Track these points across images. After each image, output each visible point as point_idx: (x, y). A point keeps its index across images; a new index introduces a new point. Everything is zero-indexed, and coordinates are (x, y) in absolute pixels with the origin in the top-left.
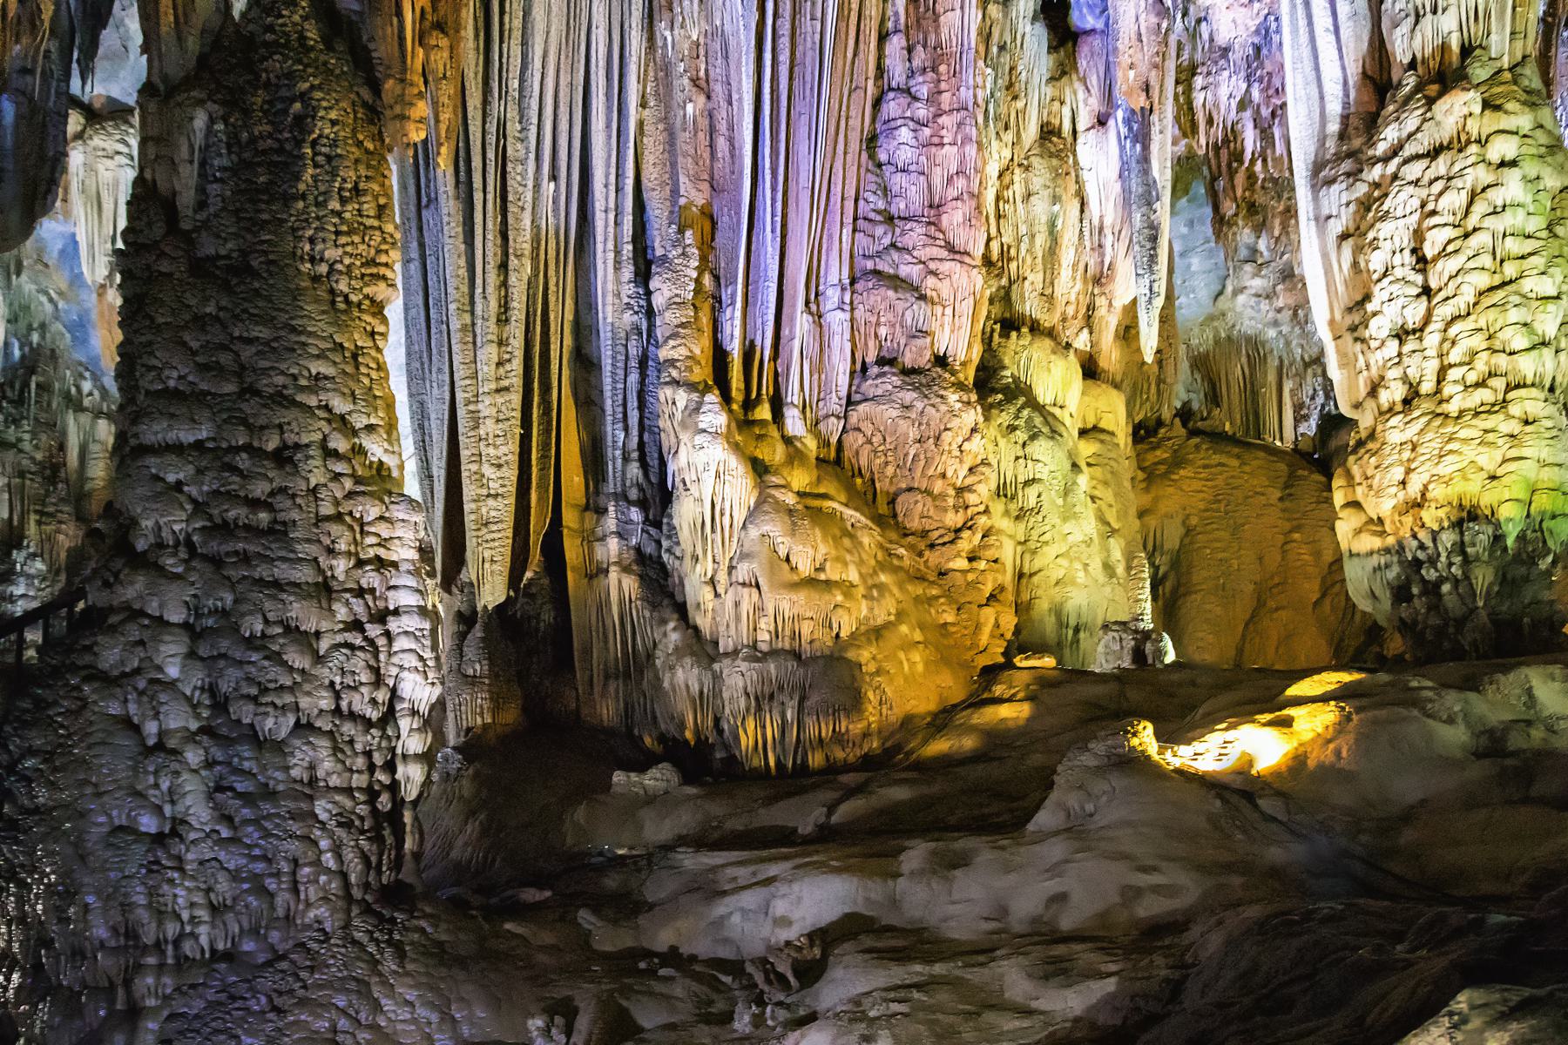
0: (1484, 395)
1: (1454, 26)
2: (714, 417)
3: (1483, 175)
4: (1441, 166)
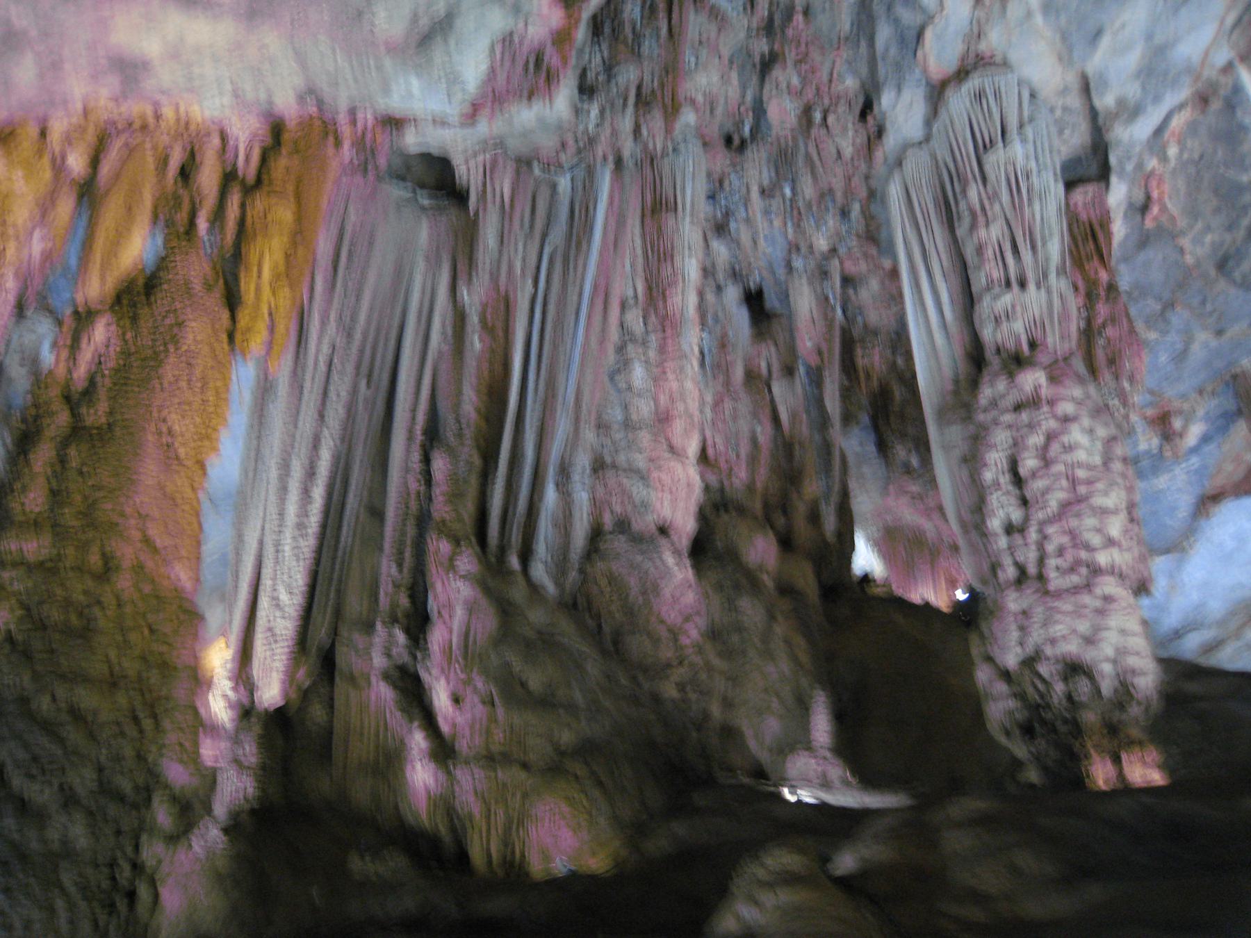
0: (1075, 579)
1: (1022, 331)
2: (467, 562)
3: (1053, 424)
4: (1025, 416)
